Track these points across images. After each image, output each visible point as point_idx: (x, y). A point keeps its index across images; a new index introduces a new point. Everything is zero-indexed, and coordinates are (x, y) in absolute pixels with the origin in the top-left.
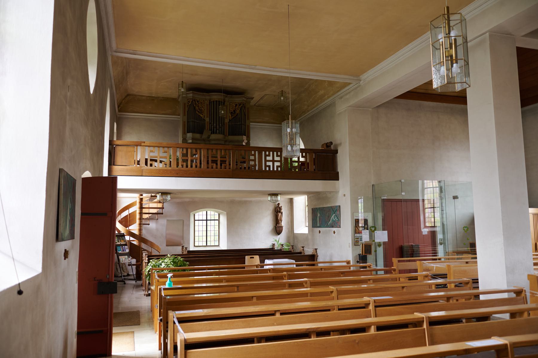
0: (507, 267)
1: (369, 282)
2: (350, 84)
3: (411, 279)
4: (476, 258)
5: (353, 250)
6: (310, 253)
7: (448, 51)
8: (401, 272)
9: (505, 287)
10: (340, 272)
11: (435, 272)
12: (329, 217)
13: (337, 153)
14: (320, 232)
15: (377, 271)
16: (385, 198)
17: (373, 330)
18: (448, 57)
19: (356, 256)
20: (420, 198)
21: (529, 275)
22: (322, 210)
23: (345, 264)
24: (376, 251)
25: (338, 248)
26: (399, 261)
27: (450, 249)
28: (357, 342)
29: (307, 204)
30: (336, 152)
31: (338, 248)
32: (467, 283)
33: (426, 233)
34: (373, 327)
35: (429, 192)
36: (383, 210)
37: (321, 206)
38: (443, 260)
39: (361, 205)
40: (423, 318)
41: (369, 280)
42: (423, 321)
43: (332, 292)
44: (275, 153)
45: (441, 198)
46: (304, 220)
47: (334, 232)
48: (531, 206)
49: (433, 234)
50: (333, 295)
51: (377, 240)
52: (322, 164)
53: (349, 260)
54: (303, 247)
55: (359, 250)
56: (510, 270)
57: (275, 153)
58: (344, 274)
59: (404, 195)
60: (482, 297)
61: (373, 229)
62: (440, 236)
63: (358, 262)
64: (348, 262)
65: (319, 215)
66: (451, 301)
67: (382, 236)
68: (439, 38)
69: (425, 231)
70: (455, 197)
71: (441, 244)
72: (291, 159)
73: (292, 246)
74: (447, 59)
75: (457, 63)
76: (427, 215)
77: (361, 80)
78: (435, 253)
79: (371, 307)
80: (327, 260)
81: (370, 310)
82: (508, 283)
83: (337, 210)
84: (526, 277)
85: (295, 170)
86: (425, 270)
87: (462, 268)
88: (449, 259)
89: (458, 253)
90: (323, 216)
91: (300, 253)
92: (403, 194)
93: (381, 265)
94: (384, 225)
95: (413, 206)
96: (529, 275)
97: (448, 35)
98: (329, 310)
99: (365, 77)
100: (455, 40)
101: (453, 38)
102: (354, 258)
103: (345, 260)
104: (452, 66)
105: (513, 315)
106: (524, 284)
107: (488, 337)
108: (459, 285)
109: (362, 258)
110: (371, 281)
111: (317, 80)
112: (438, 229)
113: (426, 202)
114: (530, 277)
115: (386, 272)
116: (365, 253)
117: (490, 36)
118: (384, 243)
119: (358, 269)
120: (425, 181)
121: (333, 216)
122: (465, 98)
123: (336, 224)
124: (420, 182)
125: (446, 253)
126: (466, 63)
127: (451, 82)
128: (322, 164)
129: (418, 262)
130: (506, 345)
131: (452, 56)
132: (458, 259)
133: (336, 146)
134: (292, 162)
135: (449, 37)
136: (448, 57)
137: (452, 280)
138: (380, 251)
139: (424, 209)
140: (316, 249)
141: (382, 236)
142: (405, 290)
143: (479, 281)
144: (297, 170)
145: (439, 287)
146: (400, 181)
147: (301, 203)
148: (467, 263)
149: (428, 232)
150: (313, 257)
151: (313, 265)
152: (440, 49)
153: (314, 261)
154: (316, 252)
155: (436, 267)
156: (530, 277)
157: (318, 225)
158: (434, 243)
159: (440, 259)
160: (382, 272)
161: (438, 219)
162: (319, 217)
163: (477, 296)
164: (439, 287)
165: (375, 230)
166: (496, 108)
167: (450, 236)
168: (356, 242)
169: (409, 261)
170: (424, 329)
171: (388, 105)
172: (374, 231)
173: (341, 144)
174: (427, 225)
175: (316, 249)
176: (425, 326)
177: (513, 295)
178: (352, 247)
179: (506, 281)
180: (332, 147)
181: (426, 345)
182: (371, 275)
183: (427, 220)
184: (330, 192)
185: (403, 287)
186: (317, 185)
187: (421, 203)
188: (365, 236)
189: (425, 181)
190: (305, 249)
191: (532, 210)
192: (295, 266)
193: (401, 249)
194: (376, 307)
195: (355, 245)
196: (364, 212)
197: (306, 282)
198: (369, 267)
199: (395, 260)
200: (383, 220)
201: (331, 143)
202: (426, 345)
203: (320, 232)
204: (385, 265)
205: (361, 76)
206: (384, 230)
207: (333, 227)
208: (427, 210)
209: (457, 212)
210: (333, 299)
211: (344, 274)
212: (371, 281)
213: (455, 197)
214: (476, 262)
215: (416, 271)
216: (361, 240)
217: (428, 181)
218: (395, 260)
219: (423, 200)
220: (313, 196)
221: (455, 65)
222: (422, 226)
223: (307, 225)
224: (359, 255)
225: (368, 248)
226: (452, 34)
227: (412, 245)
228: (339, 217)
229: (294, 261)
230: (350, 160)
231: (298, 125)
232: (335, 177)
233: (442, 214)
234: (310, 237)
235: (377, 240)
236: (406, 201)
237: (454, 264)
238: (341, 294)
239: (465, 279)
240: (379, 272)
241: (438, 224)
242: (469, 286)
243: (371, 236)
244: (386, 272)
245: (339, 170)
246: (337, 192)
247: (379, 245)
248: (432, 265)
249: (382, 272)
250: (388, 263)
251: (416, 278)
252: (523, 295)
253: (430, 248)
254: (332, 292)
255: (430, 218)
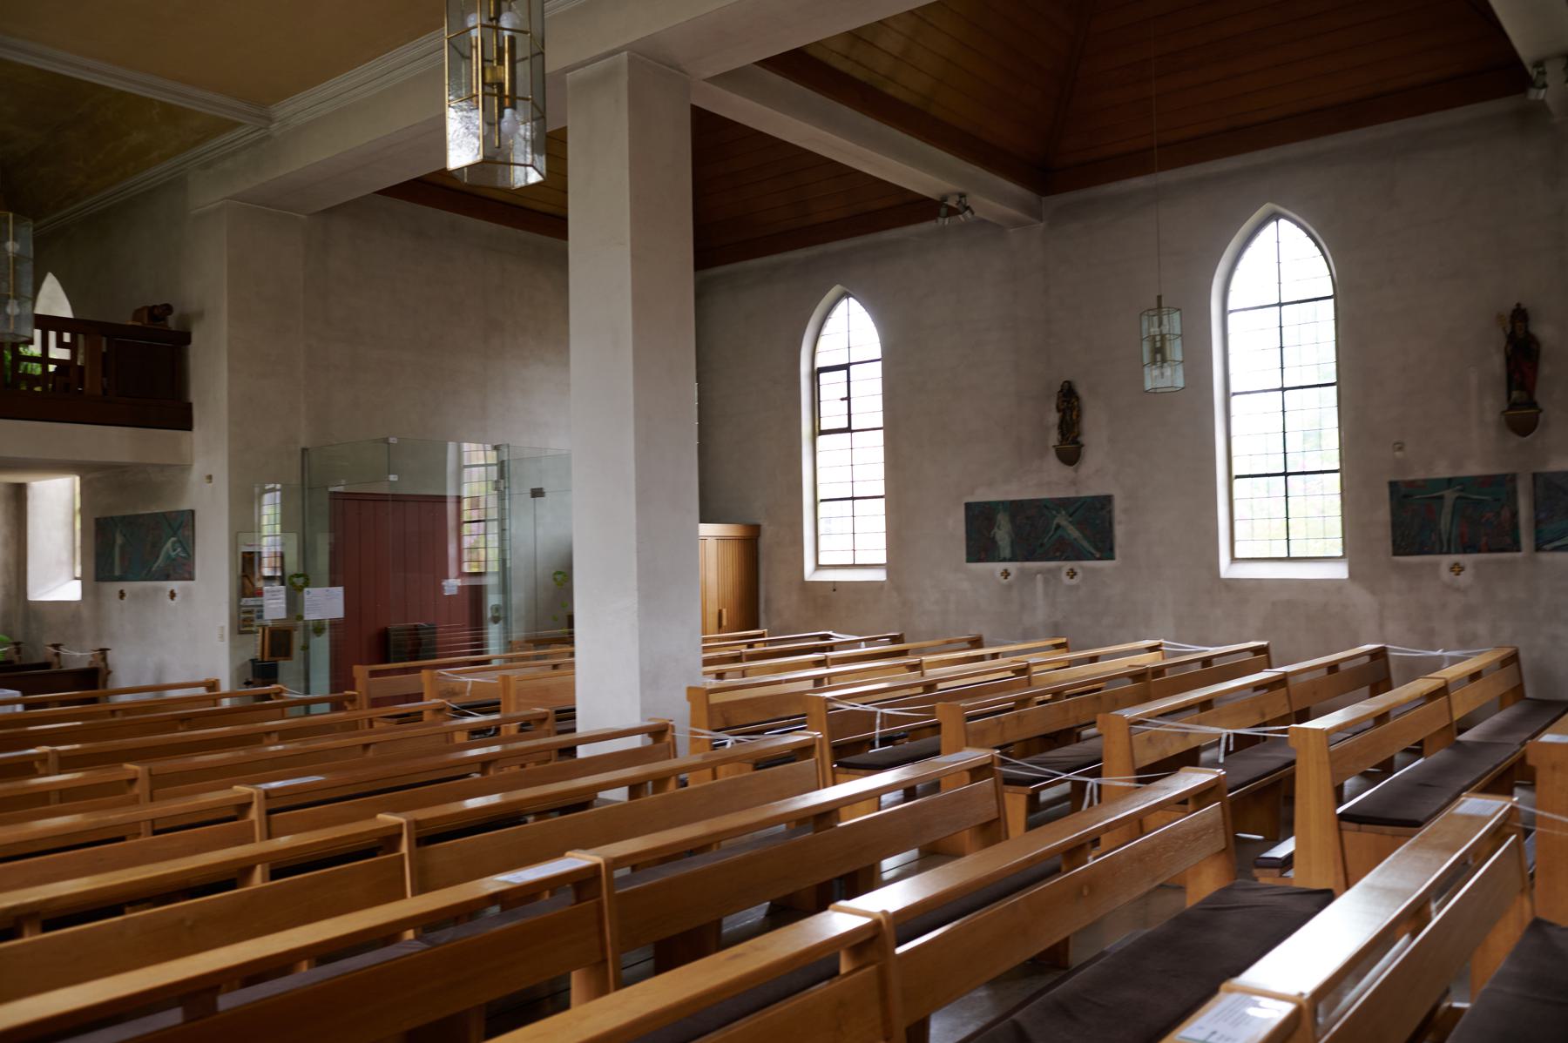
0: (643, 673)
1: (266, 741)
2: (236, 125)
3: (404, 718)
4: (572, 655)
5: (234, 648)
6: (85, 665)
7: (493, 69)
8: (376, 702)
9: (636, 721)
10: (175, 718)
11: (467, 697)
12: (156, 547)
13: (188, 341)
14: (122, 595)
15: (307, 704)
16: (340, 489)
17: (258, 880)
18: (491, 85)
19: (244, 665)
20: (451, 492)
21: (690, 689)
22: (131, 523)
23: (202, 691)
24: (306, 648)
25: (184, 641)
26: (373, 674)
27: (518, 634)
28: (189, 923)
29: (78, 505)
30: (185, 338)
31: (184, 641)
32: (542, 720)
33: (455, 592)
34: (259, 868)
35: (475, 478)
36: (333, 529)
37: (129, 512)
38: (495, 663)
39: (270, 511)
40: (401, 825)
41: (268, 734)
42: (400, 835)
43: (132, 781)
44: (52, 335)
45: (501, 498)
46: (65, 555)
47: (173, 595)
48: (704, 519)
49: (475, 594)
50: (137, 790)
51: (311, 615)
52: (134, 375)
53: (212, 677)
54: (56, 646)
55: (254, 647)
56: (650, 679)
57: (52, 335)
58: (189, 721)
59: (394, 482)
60: (583, 752)
61: (300, 581)
62: (493, 599)
63: (248, 684)
64: (212, 686)
65: (119, 540)
66: (491, 772)
67: (326, 603)
68: (470, 25)
69: (452, 585)
70: (537, 493)
71: (496, 620)
72: (14, 347)
73: (17, 644)
74: (488, 89)
75: (513, 106)
76: (467, 542)
77: (271, 120)
78: (479, 644)
79: (254, 814)
80: (148, 681)
81: (252, 822)
82: (643, 711)
83: (183, 525)
84: (683, 694)
85: (30, 388)
86: (441, 696)
87: (543, 682)
88: (511, 659)
89: (539, 643)
90: (133, 542)
91: (47, 665)
92: (393, 478)
93: (321, 685)
94: (333, 569)
95: (429, 515)
96: (690, 689)
97: (492, 24)
98: (122, 839)
99: (294, 110)
100: (512, 39)
101: (506, 33)
102: (237, 672)
103: (202, 679)
104: (501, 115)
105: (635, 789)
106: (678, 712)
107: (558, 854)
108: (526, 726)
109: (263, 671)
110: (275, 737)
111: (121, 95)
112: (491, 581)
113: (466, 504)
114: (693, 692)
115: (337, 706)
116: (272, 654)
117: (631, 61)
118: (334, 624)
119: (251, 702)
120: (466, 446)
121: (169, 544)
122: (565, 220)
123: (182, 568)
124: (451, 446)
125: (509, 645)
126: (538, 115)
127: (495, 159)
128: (134, 375)
129: (425, 673)
130: (597, 867)
131: (501, 85)
132: (537, 658)
133: (186, 320)
134: (19, 358)
135: (498, 29)
136: (491, 85)
137: (513, 713)
138: (321, 647)
139: (460, 524)
140: (103, 651)
141: (326, 603)
142: (371, 753)
143: (579, 713)
144: (38, 389)
145: (479, 734)
146: (386, 440)
147: (55, 501)
148: (555, 667)
149: (461, 588)
150: (93, 678)
151: (94, 700)
152: (470, 58)
153: (95, 687)
154: (104, 659)
155: (470, 681)
156: (693, 692)
157: (117, 573)
158: (477, 620)
159: (487, 662)
160: (326, 707)
161: (493, 554)
162: (122, 547)
163: (570, 751)
164: (479, 734)
165: (307, 585)
166: (635, 257)
167: (518, 597)
168: (243, 622)
169: (406, 671)
170: (402, 856)
171: (354, 210)
172: (301, 589)
173: (200, 315)
174: (466, 568)
175: (103, 651)
176: (404, 849)
177: (649, 741)
178: (232, 639)
179: (638, 708)
180: (172, 322)
181: (403, 896)
182: (283, 718)
183: (466, 557)
184: (162, 468)
185: (366, 746)
186: (116, 443)
187: (451, 507)
188: (274, 605)
189: (466, 446)
190: (64, 651)
191: (708, 530)
192: (19, 708)
193: (384, 637)
194: (270, 812)
195: (241, 633)
196: (282, 531)
197: (43, 758)
198: (278, 694)
199: (360, 672)
200: (333, 555)
201: (168, 309)
202: (403, 896)
203: (122, 595)
204: (336, 686)
205: (273, 107)
206: (333, 584)
207: (167, 578)
208: (466, 528)
209: (535, 531)
210: (136, 801)
211: (189, 721)
212: (275, 737)
213: (537, 493)
214: (572, 665)
215: (419, 697)
216: (260, 617)
217: (474, 446)
218: (360, 672)
219: (459, 499)
220: (100, 482)
221: (508, 112)
222: (452, 570)
223: (78, 574)
224: (253, 661)
225: (280, 641)
226: (506, 21)
227: (416, 628)
228: (188, 545)
229: (16, 694)
230: (231, 370)
231: (28, 231)
232: (181, 418)
233: (502, 539)
234: (86, 613)
235: (311, 615)
236: (398, 499)
237: (514, 674)
238: (160, 784)
239: (539, 710)
240: (314, 708)
241: (494, 567)
242: (546, 726)
243: (294, 603)
244: (337, 706)
245: (194, 397)
246: (185, 468)
247: (318, 628)
248: (464, 679)
249: (326, 707)
250: (341, 678)
251: (416, 717)
252: (668, 738)
253: (466, 634)
254: (132, 781)
255: (477, 548)
